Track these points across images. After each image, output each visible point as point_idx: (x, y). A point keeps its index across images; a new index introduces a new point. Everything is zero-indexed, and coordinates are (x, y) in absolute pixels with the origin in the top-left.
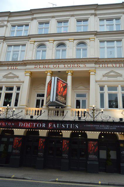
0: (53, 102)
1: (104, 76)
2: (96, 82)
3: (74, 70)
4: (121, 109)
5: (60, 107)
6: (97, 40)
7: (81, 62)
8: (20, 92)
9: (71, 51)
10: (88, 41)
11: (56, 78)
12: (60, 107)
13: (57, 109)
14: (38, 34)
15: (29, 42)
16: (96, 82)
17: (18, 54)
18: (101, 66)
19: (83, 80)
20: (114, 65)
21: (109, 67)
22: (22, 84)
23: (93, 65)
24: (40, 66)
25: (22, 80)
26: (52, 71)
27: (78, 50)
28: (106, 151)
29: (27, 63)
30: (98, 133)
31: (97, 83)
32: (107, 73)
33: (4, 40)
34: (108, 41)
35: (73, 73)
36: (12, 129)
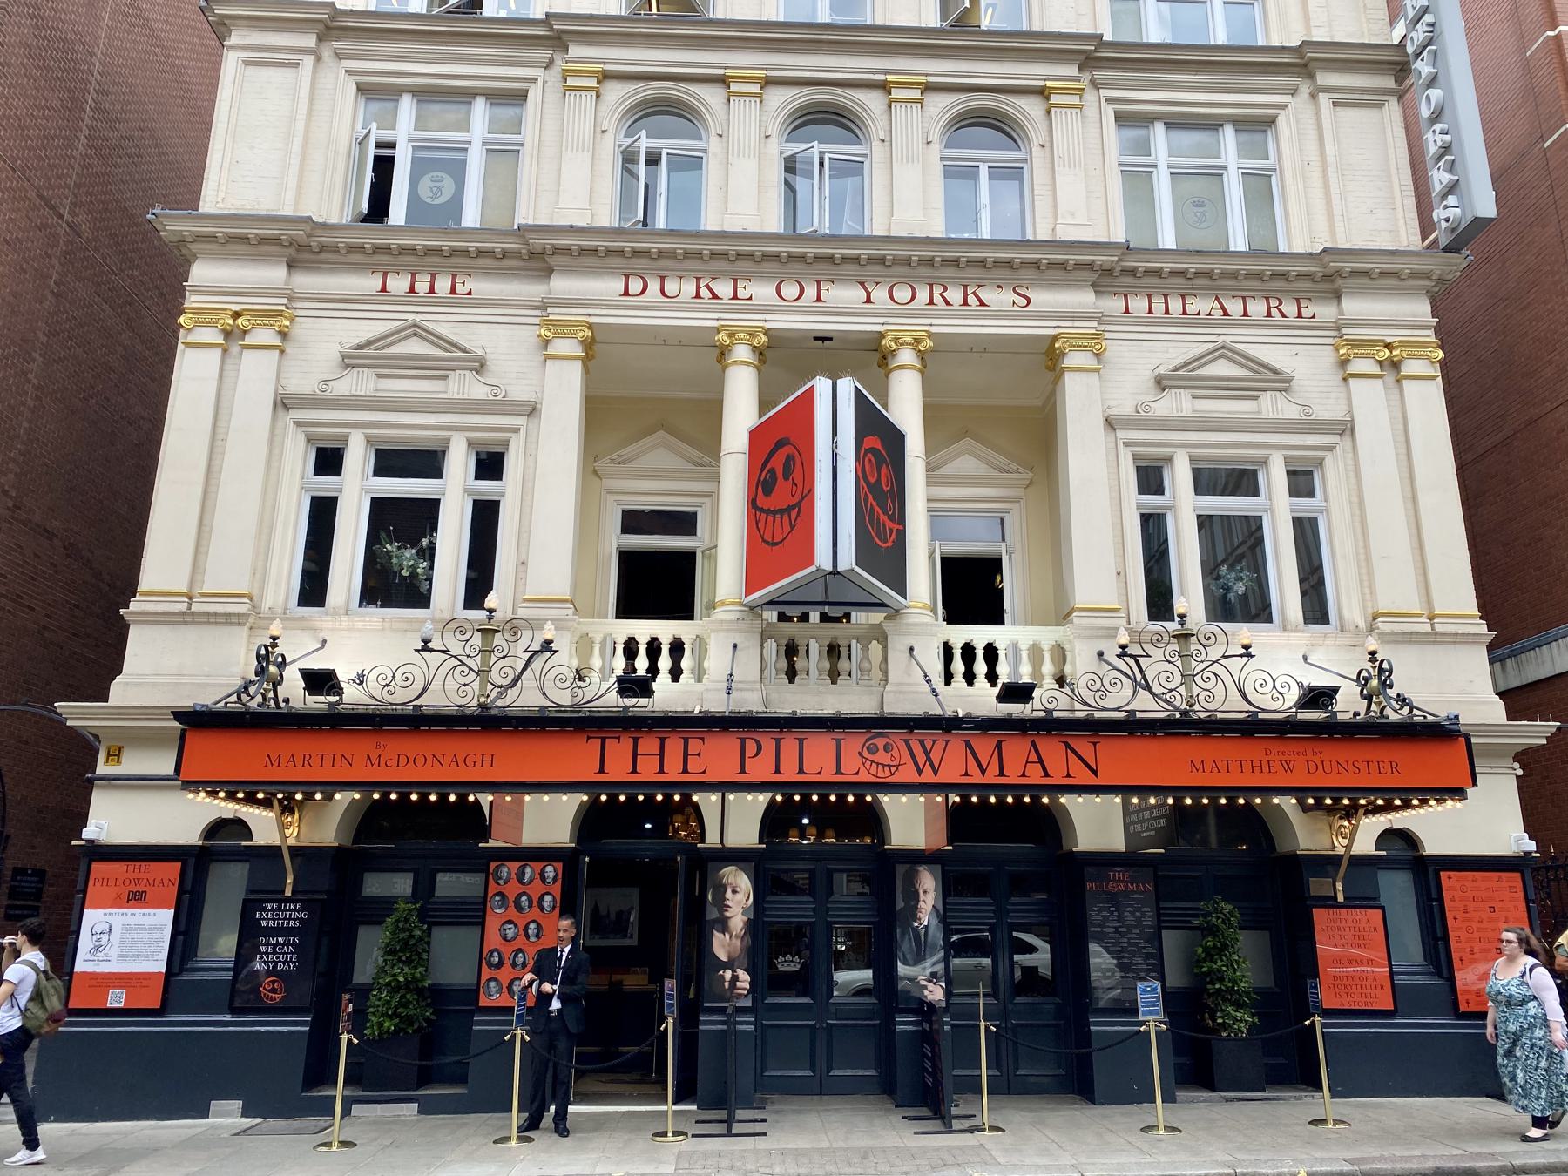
0: (835, 573)
1: (1161, 384)
2: (284, 403)
3: (945, 326)
4: (1296, 630)
5: (814, 616)
6: (1098, 111)
7: (1147, 281)
8: (508, 490)
9: (907, 184)
10: (711, 97)
11: (846, 386)
12: (814, 616)
13: (792, 629)
14: (372, 8)
15: (554, 75)
16: (1110, 424)
17: (457, 169)
18: (1139, 305)
19: (1011, 408)
20: (1234, 307)
21: (1197, 321)
22: (519, 421)
23: (1083, 299)
24: (671, 287)
25: (520, 392)
26: (767, 332)
27: (958, 172)
28: (1267, 934)
29: (557, 251)
30: (571, 803)
31: (1121, 434)
32: (1186, 364)
33: (320, 39)
34: (1176, 123)
35: (937, 358)
36: (471, 798)
